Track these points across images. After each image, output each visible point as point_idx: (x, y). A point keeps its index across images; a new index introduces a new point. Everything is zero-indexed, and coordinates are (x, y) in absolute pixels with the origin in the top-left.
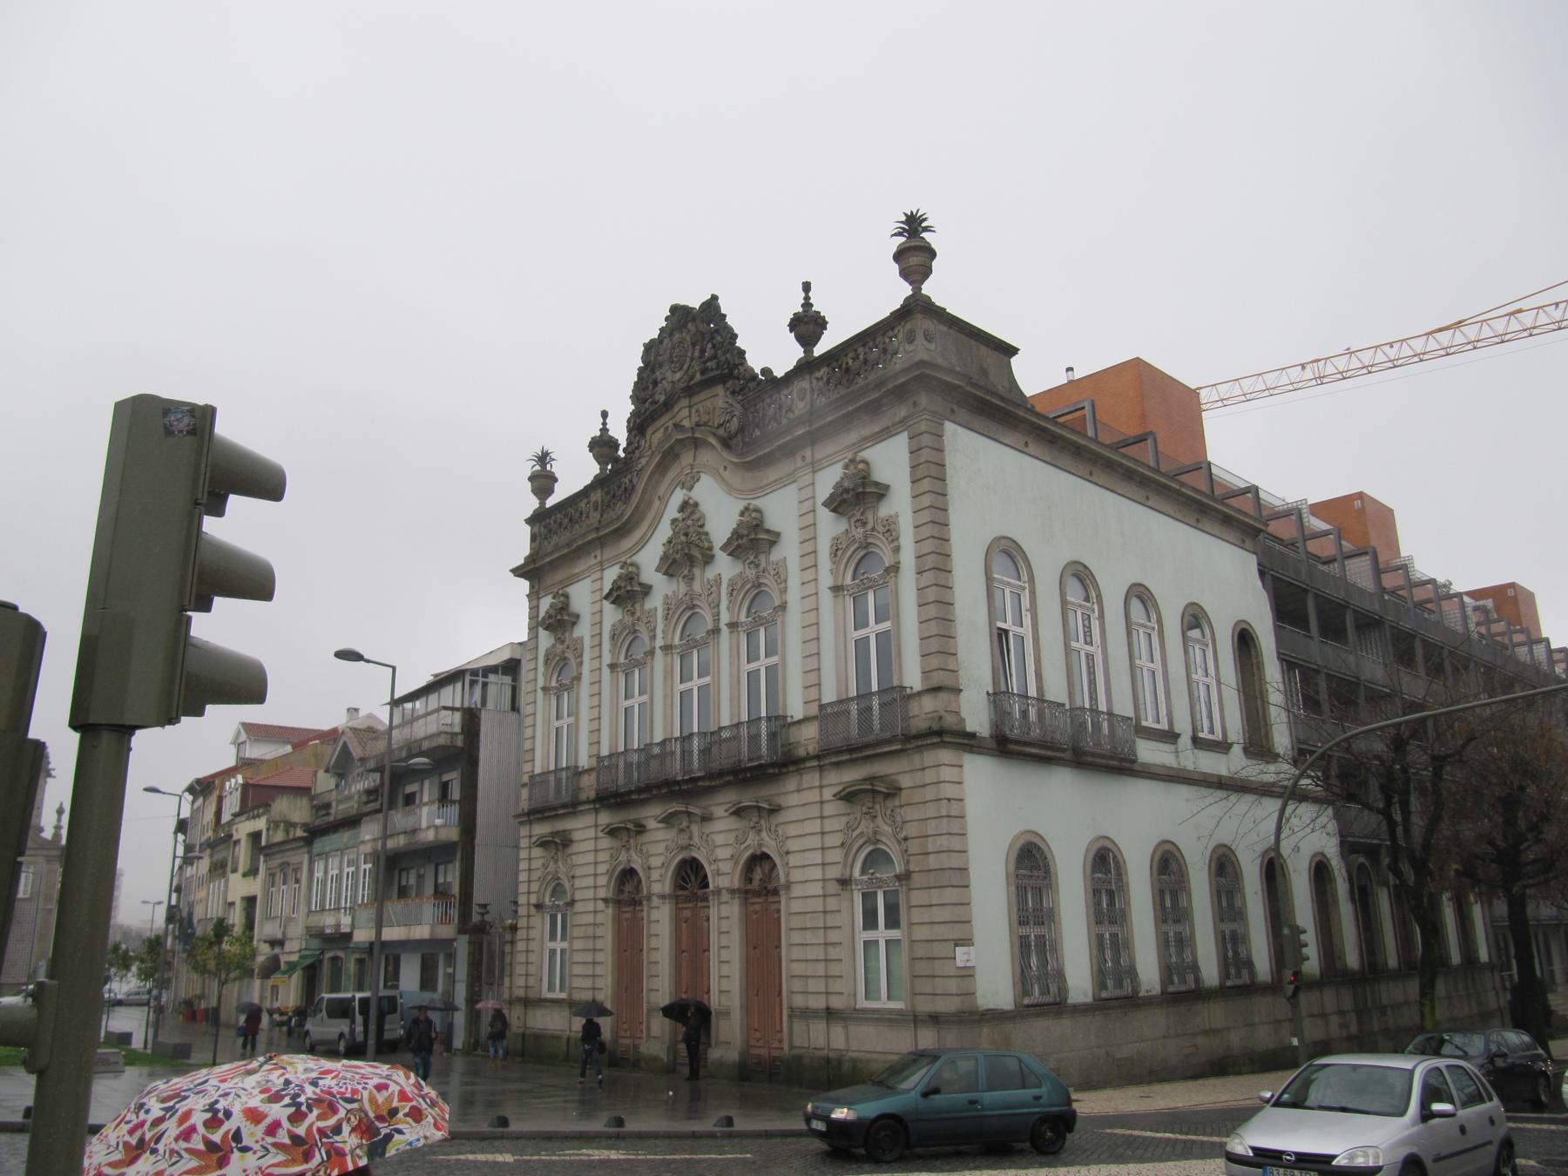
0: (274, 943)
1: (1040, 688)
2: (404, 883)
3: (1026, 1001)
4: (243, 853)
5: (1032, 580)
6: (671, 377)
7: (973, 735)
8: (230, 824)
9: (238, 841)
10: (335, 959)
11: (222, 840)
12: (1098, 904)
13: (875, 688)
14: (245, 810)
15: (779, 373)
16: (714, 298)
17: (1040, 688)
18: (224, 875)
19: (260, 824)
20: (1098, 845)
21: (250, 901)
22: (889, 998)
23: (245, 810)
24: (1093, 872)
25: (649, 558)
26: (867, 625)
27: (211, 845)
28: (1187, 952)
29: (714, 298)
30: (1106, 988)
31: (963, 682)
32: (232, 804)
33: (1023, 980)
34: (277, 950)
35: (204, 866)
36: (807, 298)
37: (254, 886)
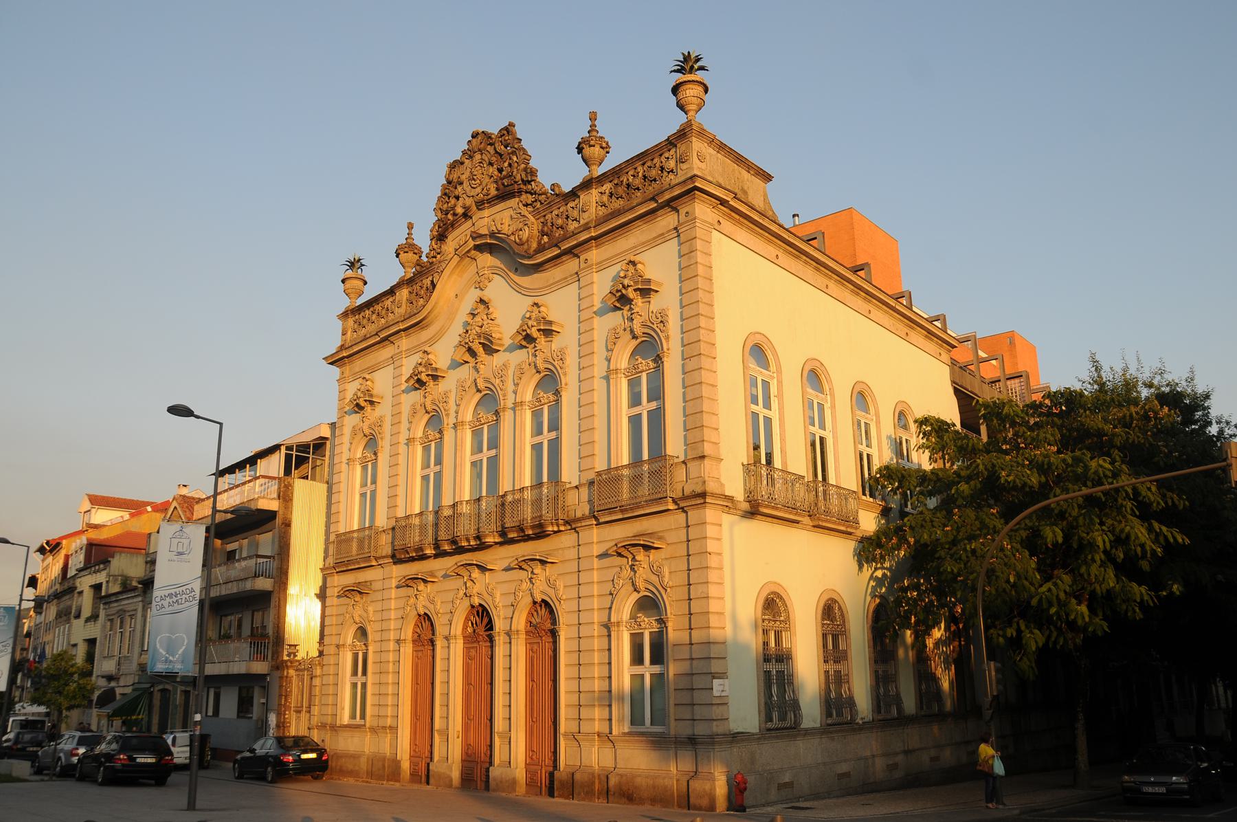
0: (110, 678)
1: (784, 462)
2: (257, 623)
3: (829, 721)
4: (86, 602)
5: (779, 371)
6: (467, 196)
7: (730, 499)
8: (74, 577)
9: (81, 593)
10: (163, 691)
11: (65, 588)
12: (825, 645)
13: (645, 457)
14: (88, 566)
15: (567, 188)
16: (512, 125)
17: (784, 462)
18: (68, 621)
19: (101, 578)
20: (826, 597)
21: (92, 642)
22: (652, 724)
23: (88, 566)
24: (823, 619)
25: (443, 353)
26: (481, 451)
27: (57, 596)
28: (845, 688)
29: (512, 125)
30: (771, 720)
31: (724, 453)
32: (78, 561)
33: (768, 709)
34: (113, 684)
35: (51, 611)
36: (593, 126)
37: (94, 630)
